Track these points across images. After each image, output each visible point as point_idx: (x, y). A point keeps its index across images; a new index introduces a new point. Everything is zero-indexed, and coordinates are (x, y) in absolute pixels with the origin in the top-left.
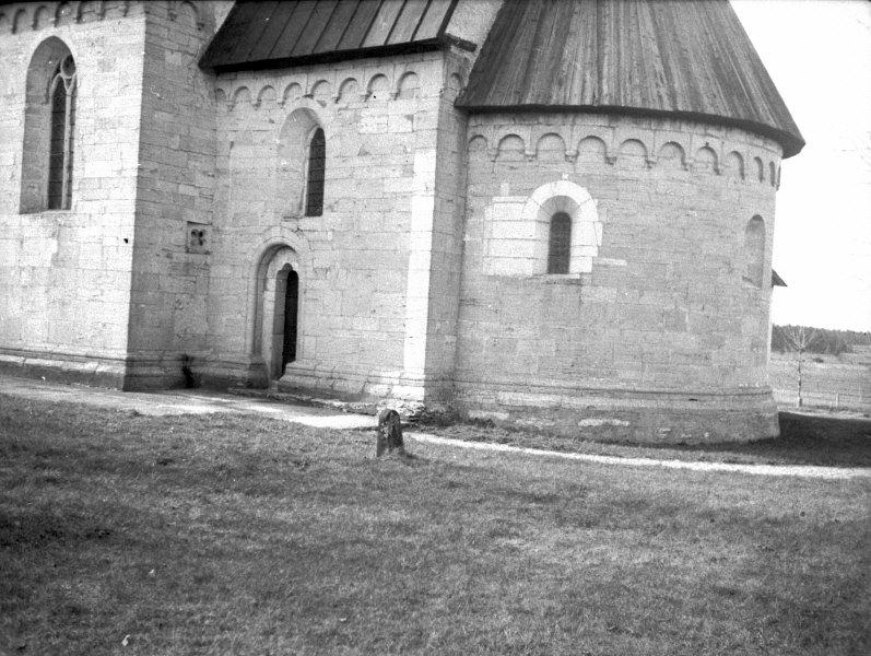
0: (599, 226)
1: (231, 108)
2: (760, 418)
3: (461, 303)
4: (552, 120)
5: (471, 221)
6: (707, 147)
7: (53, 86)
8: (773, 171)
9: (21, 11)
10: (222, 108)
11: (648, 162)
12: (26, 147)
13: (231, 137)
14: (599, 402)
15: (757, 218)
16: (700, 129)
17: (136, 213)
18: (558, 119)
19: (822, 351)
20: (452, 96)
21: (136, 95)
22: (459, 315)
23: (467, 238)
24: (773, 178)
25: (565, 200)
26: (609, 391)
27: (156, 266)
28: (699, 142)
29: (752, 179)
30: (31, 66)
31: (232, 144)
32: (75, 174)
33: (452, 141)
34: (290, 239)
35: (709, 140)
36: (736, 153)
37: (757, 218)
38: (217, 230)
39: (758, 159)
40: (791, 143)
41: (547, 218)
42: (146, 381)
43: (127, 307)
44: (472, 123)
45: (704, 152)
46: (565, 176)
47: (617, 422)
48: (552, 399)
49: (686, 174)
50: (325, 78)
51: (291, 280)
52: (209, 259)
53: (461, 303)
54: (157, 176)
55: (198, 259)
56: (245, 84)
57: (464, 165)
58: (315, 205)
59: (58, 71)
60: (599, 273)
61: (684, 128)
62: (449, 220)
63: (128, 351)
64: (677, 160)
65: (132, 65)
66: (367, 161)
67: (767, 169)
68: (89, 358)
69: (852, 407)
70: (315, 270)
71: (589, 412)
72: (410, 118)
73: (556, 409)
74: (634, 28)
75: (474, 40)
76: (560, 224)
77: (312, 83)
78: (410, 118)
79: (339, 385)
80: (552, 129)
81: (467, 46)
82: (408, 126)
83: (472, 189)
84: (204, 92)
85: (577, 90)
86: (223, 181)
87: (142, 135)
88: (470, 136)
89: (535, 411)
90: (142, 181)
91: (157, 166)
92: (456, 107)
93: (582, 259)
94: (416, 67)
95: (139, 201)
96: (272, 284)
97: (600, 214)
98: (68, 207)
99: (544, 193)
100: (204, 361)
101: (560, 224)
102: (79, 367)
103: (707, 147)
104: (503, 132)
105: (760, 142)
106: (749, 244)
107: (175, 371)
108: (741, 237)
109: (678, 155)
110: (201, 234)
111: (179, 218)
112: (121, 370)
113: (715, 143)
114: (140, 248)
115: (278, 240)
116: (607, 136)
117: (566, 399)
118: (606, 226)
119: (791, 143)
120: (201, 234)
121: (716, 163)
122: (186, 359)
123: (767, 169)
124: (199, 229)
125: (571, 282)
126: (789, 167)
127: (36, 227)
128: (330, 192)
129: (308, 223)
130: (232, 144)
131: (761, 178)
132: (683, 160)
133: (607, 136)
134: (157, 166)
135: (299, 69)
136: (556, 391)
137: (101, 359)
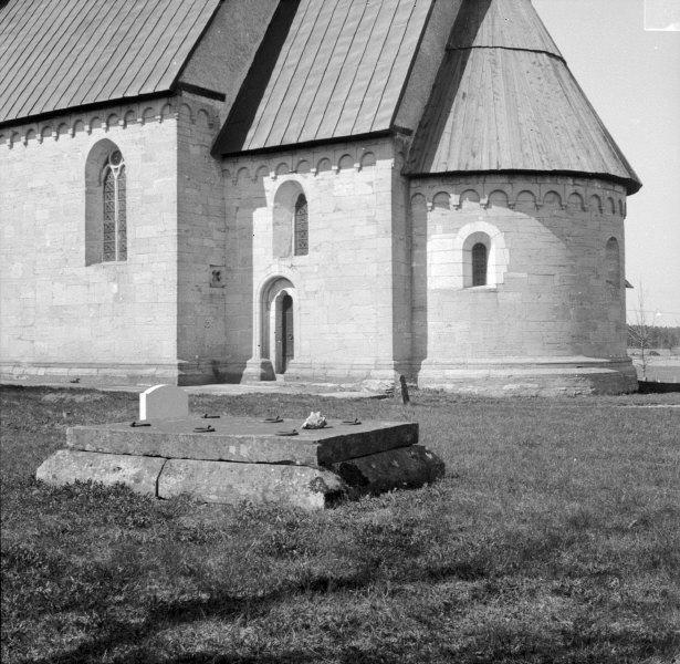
0: (507, 251)
1: (235, 183)
2: (626, 378)
3: (413, 309)
4: (469, 181)
5: (417, 252)
6: (576, 193)
7: (104, 173)
8: (621, 206)
9: (15, 134)
10: (229, 182)
11: (536, 205)
12: (87, 218)
13: (236, 204)
14: (517, 372)
15: (613, 239)
16: (570, 181)
17: (178, 261)
18: (474, 180)
19: (655, 345)
20: (399, 168)
21: (173, 179)
22: (412, 319)
23: (414, 265)
24: (621, 210)
25: (482, 234)
26: (521, 364)
27: (193, 298)
28: (570, 189)
29: (608, 213)
30: (88, 160)
31: (238, 208)
32: (129, 235)
33: (401, 197)
34: (287, 273)
35: (577, 188)
36: (596, 196)
37: (613, 239)
38: (229, 270)
39: (610, 198)
40: (632, 186)
41: (470, 248)
42: (191, 379)
43: (175, 326)
44: (413, 185)
45: (575, 197)
46: (481, 218)
47: (530, 385)
48: (483, 372)
49: (563, 213)
50: (305, 158)
51: (286, 302)
52: (225, 291)
53: (413, 309)
54: (189, 234)
55: (217, 291)
56: (244, 165)
57: (409, 214)
58: (301, 246)
59: (107, 162)
60: (506, 285)
61: (559, 181)
62: (402, 255)
63: (179, 358)
64: (556, 204)
65: (169, 156)
66: (339, 215)
67: (617, 204)
68: (150, 365)
69: (676, 380)
70: (306, 293)
71: (509, 379)
72: (370, 184)
73: (487, 378)
74: (494, 126)
75: (410, 127)
76: (478, 252)
77: (296, 162)
78: (370, 184)
79: (330, 373)
80: (471, 187)
81: (407, 132)
82: (370, 190)
83: (415, 230)
84: (215, 172)
85: (485, 158)
86: (231, 234)
87: (179, 206)
88: (412, 194)
89: (472, 381)
90: (182, 238)
91: (189, 227)
92: (403, 175)
93: (493, 276)
94: (372, 149)
95: (180, 253)
96: (273, 305)
97: (506, 243)
98: (124, 257)
99: (467, 230)
100: (226, 364)
101: (478, 252)
102: (140, 372)
103: (576, 193)
104: (436, 190)
105: (611, 187)
106: (608, 257)
107: (209, 372)
108: (603, 253)
109: (557, 199)
110: (218, 274)
111: (204, 262)
112: (175, 373)
113: (581, 190)
114: (181, 285)
115: (276, 274)
116: (508, 189)
117: (493, 371)
118: (511, 250)
119: (632, 186)
120: (218, 274)
121: (582, 204)
122: (214, 363)
123: (617, 204)
124: (217, 270)
125: (490, 291)
126: (631, 200)
127: (98, 273)
128: (312, 239)
129: (299, 260)
130: (238, 208)
131: (614, 212)
132: (560, 203)
133: (508, 189)
134: (189, 227)
135: (285, 153)
136: (486, 366)
137: (157, 365)
